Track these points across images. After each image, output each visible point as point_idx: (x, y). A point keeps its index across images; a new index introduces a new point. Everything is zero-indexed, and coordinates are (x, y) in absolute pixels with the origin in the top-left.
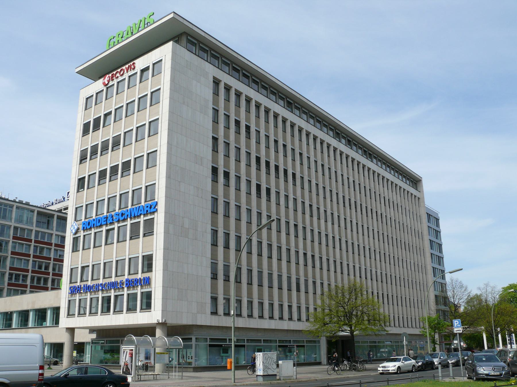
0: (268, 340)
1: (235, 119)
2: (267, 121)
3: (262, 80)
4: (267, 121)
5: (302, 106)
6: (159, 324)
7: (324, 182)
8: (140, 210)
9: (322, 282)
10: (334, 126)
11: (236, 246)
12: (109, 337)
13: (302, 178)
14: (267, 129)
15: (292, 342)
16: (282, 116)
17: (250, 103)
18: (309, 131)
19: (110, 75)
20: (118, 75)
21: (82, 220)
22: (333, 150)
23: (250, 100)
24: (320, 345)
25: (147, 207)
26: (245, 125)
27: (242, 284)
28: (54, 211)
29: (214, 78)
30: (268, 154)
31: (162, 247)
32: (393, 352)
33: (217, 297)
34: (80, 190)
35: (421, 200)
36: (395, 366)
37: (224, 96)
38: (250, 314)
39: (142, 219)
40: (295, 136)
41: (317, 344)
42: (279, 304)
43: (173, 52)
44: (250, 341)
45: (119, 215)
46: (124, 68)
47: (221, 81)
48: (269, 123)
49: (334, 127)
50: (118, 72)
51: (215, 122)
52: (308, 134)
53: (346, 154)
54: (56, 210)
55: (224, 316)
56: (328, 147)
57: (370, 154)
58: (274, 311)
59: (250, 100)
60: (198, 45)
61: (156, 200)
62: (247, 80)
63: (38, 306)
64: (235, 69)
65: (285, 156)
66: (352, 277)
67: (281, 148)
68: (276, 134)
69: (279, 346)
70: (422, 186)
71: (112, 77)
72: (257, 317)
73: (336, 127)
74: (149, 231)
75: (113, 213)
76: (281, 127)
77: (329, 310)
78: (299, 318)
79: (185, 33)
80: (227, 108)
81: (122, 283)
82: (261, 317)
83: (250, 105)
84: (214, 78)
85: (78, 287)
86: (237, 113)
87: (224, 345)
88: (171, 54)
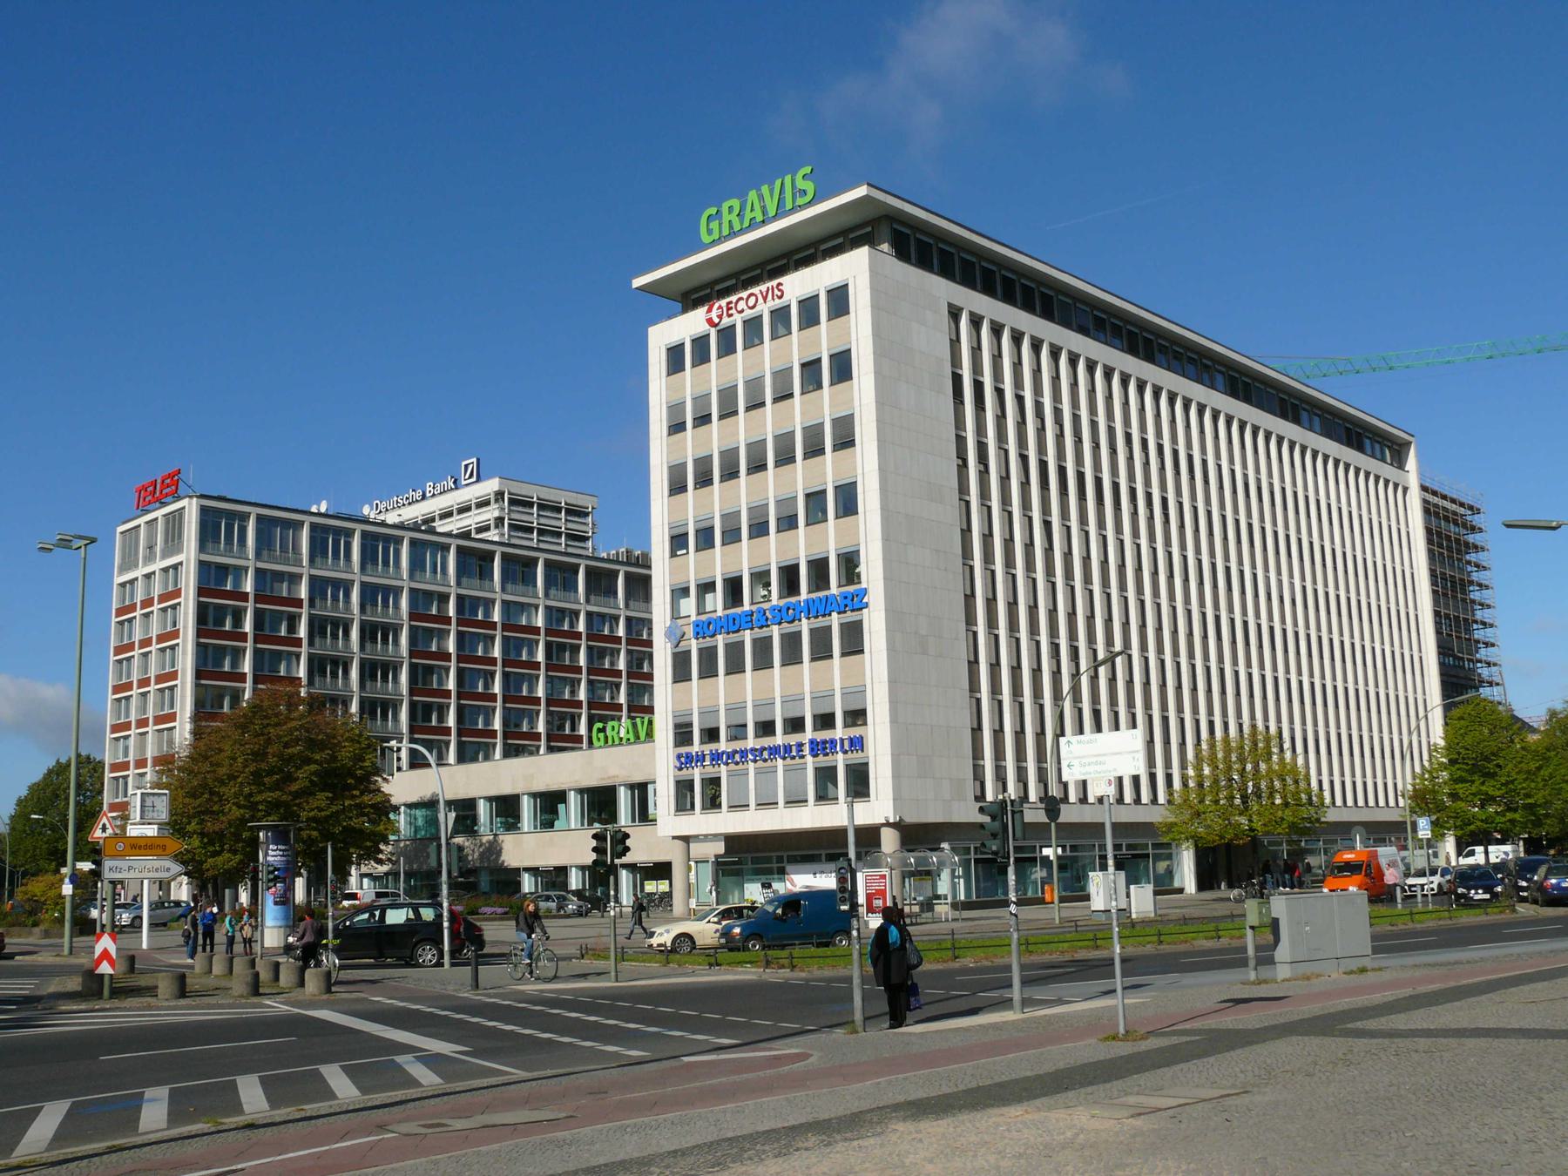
6: (888, 824)
8: (829, 604)
12: (758, 851)
19: (723, 302)
20: (742, 305)
21: (689, 616)
25: (846, 598)
28: (449, 535)
29: (950, 305)
31: (886, 680)
34: (679, 553)
36: (168, 870)
39: (835, 620)
43: (871, 271)
45: (780, 611)
46: (756, 290)
50: (741, 299)
54: (454, 532)
56: (1186, 408)
61: (864, 585)
63: (541, 786)
66: (1288, 755)
71: (729, 309)
74: (854, 642)
75: (765, 606)
81: (800, 746)
84: (950, 305)
85: (697, 756)
88: (867, 274)
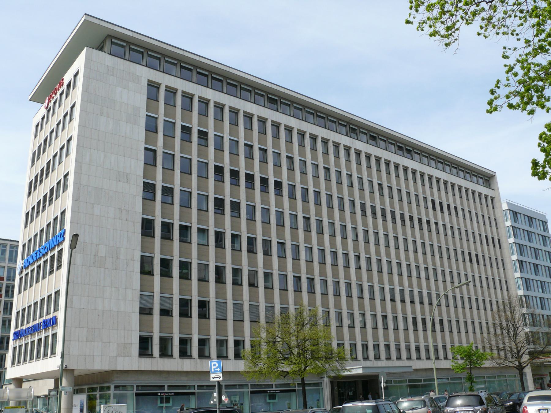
0: (203, 386)
1: (432, 199)
2: (379, 170)
3: (212, 72)
4: (379, 170)
5: (414, 148)
7: (458, 224)
9: (487, 322)
10: (347, 121)
11: (370, 295)
13: (459, 229)
14: (359, 171)
15: (393, 382)
16: (365, 152)
17: (252, 119)
18: (303, 129)
22: (478, 195)
23: (360, 152)
24: (322, 389)
26: (439, 203)
27: (192, 319)
30: (419, 213)
32: (445, 392)
33: (419, 345)
35: (495, 201)
37: (345, 157)
38: (399, 357)
40: (433, 187)
41: (320, 388)
42: (385, 345)
44: (278, 386)
47: (306, 132)
48: (350, 161)
49: (347, 122)
51: (327, 180)
52: (430, 177)
53: (465, 188)
55: (397, 360)
57: (407, 150)
58: (357, 352)
59: (360, 152)
60: (253, 92)
62: (409, 155)
64: (400, 148)
65: (418, 205)
67: (284, 162)
68: (398, 184)
69: (411, 386)
70: (497, 182)
72: (425, 359)
73: (350, 122)
76: (428, 184)
77: (497, 347)
78: (445, 357)
79: (109, 36)
80: (337, 165)
82: (437, 358)
83: (416, 176)
86: (380, 178)
87: (269, 391)
